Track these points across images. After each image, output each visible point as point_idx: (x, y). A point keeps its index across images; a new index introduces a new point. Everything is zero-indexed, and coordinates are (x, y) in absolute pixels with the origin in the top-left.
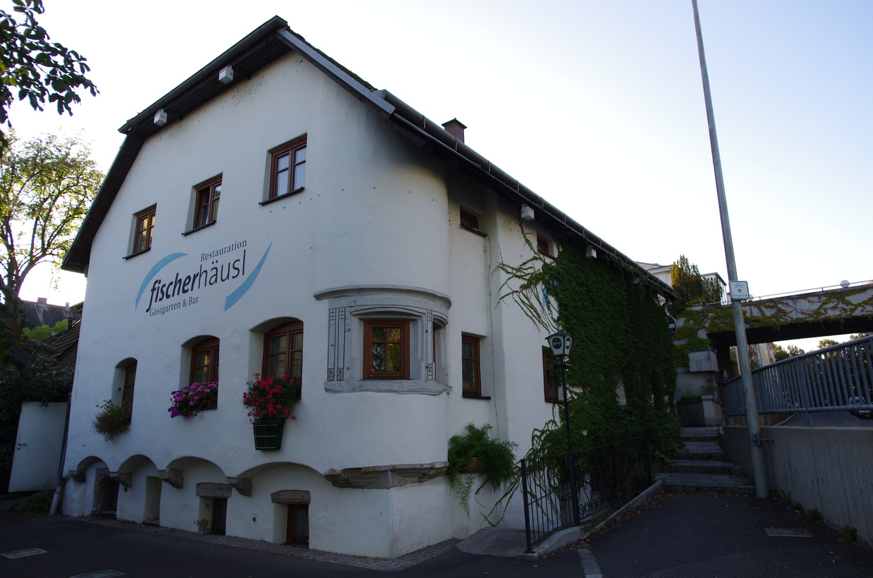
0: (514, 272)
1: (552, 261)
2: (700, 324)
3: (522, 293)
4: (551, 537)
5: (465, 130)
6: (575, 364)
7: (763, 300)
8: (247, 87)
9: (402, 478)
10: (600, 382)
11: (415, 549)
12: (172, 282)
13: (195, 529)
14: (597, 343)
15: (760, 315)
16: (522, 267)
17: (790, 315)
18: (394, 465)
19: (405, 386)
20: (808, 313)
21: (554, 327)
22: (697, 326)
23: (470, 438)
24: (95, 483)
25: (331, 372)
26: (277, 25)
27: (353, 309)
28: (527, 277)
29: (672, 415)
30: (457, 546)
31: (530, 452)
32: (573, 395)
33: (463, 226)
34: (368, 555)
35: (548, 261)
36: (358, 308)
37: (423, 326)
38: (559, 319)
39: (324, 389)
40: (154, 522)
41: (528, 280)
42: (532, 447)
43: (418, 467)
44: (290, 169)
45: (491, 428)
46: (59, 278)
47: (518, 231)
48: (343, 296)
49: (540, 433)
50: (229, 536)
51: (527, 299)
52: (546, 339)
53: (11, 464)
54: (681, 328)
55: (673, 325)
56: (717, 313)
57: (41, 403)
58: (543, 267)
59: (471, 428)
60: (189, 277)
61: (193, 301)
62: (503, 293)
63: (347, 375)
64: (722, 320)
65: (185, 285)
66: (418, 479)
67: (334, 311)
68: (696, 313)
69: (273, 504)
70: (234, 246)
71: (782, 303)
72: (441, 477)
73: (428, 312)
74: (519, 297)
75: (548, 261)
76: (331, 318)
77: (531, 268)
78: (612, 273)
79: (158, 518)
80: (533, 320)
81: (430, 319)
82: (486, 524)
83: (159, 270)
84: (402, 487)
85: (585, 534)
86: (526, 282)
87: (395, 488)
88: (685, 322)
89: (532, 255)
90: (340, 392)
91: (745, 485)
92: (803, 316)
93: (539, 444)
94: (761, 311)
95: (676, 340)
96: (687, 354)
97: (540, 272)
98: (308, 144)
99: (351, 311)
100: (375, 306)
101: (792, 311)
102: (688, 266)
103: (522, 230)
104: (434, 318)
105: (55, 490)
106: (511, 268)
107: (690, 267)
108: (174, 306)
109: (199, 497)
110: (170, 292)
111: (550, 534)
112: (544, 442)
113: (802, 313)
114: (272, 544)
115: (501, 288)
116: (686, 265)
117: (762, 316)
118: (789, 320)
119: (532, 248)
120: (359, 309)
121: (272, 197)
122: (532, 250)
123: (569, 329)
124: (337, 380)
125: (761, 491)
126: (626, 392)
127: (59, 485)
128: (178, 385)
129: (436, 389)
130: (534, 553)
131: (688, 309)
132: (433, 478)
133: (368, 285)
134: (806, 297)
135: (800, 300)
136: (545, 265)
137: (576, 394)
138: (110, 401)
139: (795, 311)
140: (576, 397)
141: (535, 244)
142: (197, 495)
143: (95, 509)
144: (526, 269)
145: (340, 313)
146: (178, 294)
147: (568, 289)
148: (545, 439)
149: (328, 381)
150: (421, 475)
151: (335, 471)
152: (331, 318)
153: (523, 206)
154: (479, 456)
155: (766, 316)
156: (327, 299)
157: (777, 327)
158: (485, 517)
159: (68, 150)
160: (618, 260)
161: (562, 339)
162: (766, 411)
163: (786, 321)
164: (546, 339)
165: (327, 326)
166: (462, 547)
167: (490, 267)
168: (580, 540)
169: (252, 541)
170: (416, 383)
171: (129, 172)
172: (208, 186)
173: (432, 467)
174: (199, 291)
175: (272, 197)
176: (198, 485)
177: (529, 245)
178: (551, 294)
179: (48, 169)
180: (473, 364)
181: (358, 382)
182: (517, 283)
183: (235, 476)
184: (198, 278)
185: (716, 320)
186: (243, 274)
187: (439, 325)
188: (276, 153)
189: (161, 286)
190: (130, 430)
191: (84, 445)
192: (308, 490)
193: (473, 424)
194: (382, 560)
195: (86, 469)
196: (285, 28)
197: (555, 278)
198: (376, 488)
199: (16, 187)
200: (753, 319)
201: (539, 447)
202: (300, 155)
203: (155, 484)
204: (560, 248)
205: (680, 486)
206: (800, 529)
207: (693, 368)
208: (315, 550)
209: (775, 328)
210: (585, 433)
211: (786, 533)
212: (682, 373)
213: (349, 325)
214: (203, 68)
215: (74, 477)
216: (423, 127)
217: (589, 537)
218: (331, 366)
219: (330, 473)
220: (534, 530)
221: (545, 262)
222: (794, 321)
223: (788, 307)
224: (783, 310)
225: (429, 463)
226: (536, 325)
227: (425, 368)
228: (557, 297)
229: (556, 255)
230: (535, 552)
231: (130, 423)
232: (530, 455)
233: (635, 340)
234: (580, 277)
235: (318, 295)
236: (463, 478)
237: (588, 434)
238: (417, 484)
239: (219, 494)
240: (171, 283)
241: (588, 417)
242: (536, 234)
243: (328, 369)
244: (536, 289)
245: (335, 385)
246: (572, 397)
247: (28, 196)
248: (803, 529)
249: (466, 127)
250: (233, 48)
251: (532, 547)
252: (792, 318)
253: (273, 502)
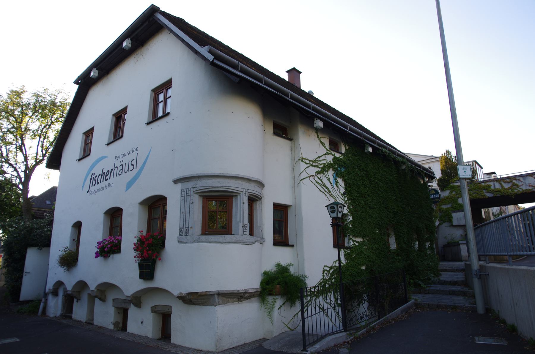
0: (311, 163)
1: (340, 155)
2: (460, 194)
3: (317, 177)
4: (323, 340)
5: (301, 74)
6: (357, 222)
7: (502, 178)
8: (141, 51)
9: (225, 299)
10: (376, 234)
11: (235, 346)
12: (100, 174)
13: (111, 327)
14: (373, 209)
15: (500, 188)
16: (317, 159)
17: (521, 187)
18: (219, 291)
19: (227, 239)
20: (533, 185)
21: (341, 198)
22: (457, 195)
23: (277, 272)
24: (62, 297)
25: (181, 230)
26: (153, 10)
27: (195, 190)
28: (321, 166)
29: (432, 255)
30: (262, 344)
31: (321, 281)
32: (355, 243)
33: (275, 134)
34: (202, 349)
35: (337, 155)
36: (198, 189)
37: (241, 200)
38: (345, 193)
39: (177, 241)
40: (91, 322)
41: (322, 168)
42: (322, 278)
43: (235, 292)
44: (163, 101)
45: (293, 265)
46: (50, 173)
47: (315, 136)
48: (189, 181)
49: (329, 268)
50: (128, 332)
51: (321, 180)
52: (325, 207)
53: (21, 284)
54: (446, 197)
55: (438, 195)
56: (471, 187)
57: (38, 248)
58: (333, 160)
59: (278, 265)
60: (108, 171)
61: (110, 186)
62: (302, 176)
63: (190, 232)
64: (474, 191)
65: (106, 176)
66: (238, 300)
67: (184, 191)
68: (457, 187)
69: (152, 313)
70: (132, 151)
71: (516, 180)
72: (256, 298)
73: (245, 190)
74: (315, 180)
75: (337, 155)
76: (182, 195)
77: (324, 160)
78: (385, 162)
79: (93, 320)
80: (325, 194)
81: (246, 195)
82: (286, 329)
83: (94, 167)
84: (225, 305)
85: (349, 338)
86: (320, 170)
87: (220, 306)
88: (449, 193)
89: (325, 151)
90: (186, 243)
91: (471, 304)
92: (530, 188)
93: (328, 276)
94: (501, 185)
95: (444, 204)
96: (451, 214)
97: (331, 163)
98: (172, 86)
99: (194, 191)
100: (209, 187)
101: (523, 184)
102: (451, 157)
103: (317, 135)
104: (249, 194)
105: (41, 300)
106: (308, 160)
107: (453, 157)
108: (101, 189)
109: (114, 308)
110: (99, 181)
111: (323, 337)
112: (332, 274)
113: (530, 186)
114: (151, 339)
115: (301, 173)
116: (450, 156)
117: (502, 188)
118: (521, 190)
119: (325, 147)
120: (198, 189)
121: (154, 118)
122: (325, 149)
123: (352, 199)
124: (185, 235)
125: (481, 310)
126: (396, 240)
127: (44, 298)
128: (102, 238)
129: (249, 240)
130: (307, 351)
131: (451, 184)
132: (250, 298)
133: (204, 174)
134: (532, 175)
135: (528, 177)
136: (335, 158)
137: (357, 242)
138: (68, 247)
139: (525, 184)
140: (357, 244)
141: (327, 144)
142: (113, 306)
143: (62, 313)
144: (321, 161)
145: (187, 192)
146: (103, 182)
147: (351, 174)
148: (333, 272)
149: (180, 236)
150: (239, 297)
151: (182, 294)
152: (182, 195)
153: (315, 119)
154: (281, 284)
155: (505, 188)
156: (180, 183)
157: (512, 195)
158: (286, 324)
159: (56, 97)
160: (389, 153)
161: (335, 207)
162: (486, 254)
163: (518, 191)
164: (325, 207)
165: (180, 200)
166: (266, 345)
167: (294, 160)
168: (345, 342)
169: (140, 336)
170: (235, 237)
171: (81, 108)
172: (120, 114)
173: (246, 292)
174: (114, 180)
175: (154, 118)
176: (114, 300)
177: (323, 145)
178: (339, 177)
179: (44, 108)
180: (283, 224)
181: (197, 237)
182: (313, 170)
183: (130, 296)
184: (113, 171)
185: (471, 191)
186: (136, 168)
187: (253, 200)
188: (156, 92)
189: (94, 176)
190: (77, 265)
191: (56, 274)
192: (171, 305)
193: (280, 262)
194: (210, 353)
195: (58, 288)
196: (158, 12)
197: (342, 166)
198: (208, 306)
199: (26, 119)
200: (496, 191)
201: (328, 278)
202: (170, 92)
203: (92, 298)
204: (347, 146)
205: (426, 304)
206: (500, 338)
207: (455, 223)
208: (174, 344)
209: (511, 196)
210: (364, 268)
211: (489, 341)
212: (448, 226)
213: (193, 200)
214: (115, 41)
215: (51, 292)
216: (238, 70)
217: (351, 340)
218: (182, 226)
219: (179, 296)
220: (317, 334)
221: (335, 156)
222: (524, 191)
223: (520, 182)
224: (517, 184)
225: (244, 289)
226: (328, 197)
227: (242, 227)
228: (344, 179)
229: (343, 151)
230: (308, 351)
231: (77, 261)
232: (321, 283)
233: (403, 206)
234: (361, 165)
235: (175, 180)
236: (270, 299)
237: (366, 269)
238: (237, 303)
239: (124, 306)
240: (100, 175)
241: (365, 257)
242: (328, 138)
243: (180, 228)
244: (328, 173)
245: (183, 238)
246: (354, 244)
247: (34, 125)
248: (502, 339)
249: (301, 73)
250: (130, 27)
251: (307, 347)
252: (522, 189)
253: (152, 312)
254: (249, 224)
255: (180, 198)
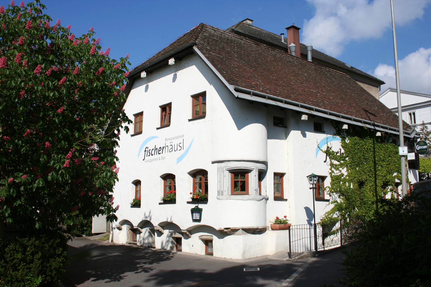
5: (299, 30)
25: (219, 192)
27: (226, 168)
55: (426, 146)
60: (160, 148)
61: (163, 158)
65: (159, 151)
110: (153, 153)
146: (156, 154)
151: (221, 228)
152: (218, 171)
174: (165, 154)
184: (164, 148)
189: (148, 150)
240: (153, 149)
254: (259, 188)
255: (217, 173)
